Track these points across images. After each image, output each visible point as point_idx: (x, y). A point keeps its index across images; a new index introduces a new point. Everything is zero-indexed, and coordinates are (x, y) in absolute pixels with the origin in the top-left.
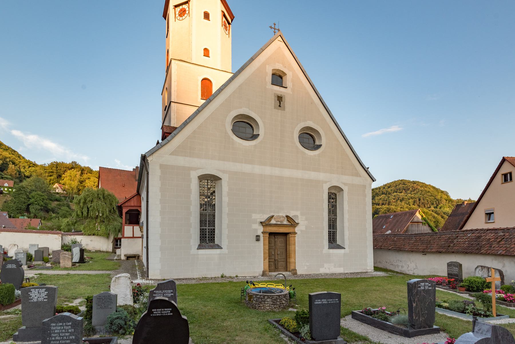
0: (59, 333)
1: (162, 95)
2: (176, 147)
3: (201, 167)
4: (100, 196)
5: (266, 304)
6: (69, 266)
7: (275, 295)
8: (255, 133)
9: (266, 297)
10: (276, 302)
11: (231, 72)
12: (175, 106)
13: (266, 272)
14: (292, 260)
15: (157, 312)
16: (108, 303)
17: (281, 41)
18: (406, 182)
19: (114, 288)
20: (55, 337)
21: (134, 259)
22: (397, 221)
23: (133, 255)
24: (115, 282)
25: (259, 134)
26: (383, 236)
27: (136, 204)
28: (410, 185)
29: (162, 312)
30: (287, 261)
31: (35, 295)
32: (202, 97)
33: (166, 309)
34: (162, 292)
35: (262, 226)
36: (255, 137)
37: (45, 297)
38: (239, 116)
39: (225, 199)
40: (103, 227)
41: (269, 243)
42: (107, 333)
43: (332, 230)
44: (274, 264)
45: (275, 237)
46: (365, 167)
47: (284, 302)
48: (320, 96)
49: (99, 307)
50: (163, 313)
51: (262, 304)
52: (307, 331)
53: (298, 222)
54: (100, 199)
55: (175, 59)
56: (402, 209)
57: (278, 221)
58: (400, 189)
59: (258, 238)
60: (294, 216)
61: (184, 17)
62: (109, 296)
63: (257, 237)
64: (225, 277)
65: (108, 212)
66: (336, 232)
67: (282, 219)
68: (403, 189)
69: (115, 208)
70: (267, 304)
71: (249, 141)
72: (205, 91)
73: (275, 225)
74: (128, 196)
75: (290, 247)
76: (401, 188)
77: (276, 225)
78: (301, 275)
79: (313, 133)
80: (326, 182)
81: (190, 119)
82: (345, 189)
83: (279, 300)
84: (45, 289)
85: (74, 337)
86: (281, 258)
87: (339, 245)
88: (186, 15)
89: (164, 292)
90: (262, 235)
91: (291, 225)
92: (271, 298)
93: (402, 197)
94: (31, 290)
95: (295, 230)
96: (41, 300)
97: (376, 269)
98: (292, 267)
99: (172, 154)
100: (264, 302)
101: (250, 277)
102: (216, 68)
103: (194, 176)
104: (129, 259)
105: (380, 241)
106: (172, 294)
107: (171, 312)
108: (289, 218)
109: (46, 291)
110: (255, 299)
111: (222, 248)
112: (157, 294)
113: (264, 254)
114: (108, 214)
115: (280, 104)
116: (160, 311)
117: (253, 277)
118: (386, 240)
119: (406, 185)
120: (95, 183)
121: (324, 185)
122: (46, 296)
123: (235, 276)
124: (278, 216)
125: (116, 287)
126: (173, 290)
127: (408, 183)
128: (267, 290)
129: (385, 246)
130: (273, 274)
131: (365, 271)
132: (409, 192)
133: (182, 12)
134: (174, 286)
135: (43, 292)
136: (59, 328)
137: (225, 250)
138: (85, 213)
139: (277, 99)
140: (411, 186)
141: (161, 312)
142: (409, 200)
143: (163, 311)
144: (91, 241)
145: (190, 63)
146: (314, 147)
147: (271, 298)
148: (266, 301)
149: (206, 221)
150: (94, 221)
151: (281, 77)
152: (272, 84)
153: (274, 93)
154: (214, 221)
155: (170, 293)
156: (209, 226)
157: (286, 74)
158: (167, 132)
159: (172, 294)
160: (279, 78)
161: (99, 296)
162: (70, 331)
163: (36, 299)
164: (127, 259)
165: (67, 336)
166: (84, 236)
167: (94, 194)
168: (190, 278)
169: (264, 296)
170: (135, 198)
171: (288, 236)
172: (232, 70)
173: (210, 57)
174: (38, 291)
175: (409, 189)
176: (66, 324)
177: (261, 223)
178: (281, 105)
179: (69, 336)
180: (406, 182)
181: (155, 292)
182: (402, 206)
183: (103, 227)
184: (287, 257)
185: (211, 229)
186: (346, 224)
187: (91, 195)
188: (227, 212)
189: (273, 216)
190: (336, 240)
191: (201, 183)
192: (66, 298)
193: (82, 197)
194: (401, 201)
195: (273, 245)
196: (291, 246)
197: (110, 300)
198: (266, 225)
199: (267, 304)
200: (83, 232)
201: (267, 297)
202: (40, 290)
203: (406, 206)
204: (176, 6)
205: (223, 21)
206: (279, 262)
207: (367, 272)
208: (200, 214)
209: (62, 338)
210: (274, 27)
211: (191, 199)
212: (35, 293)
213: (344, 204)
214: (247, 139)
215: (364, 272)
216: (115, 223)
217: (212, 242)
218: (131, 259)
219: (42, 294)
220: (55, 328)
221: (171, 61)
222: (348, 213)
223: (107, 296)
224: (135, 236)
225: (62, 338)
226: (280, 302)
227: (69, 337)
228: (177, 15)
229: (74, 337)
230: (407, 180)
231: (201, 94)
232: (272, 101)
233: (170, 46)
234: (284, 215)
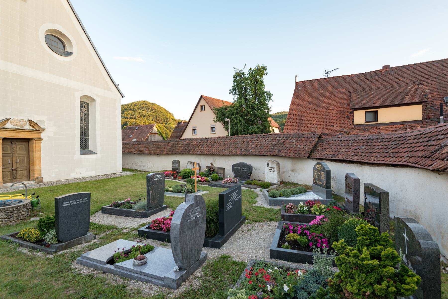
7: (10, 207)
14: (36, 168)
22: (141, 132)
30: (30, 169)
44: (11, 173)
45: (12, 143)
46: (116, 84)
57: (17, 126)
60: (39, 121)
66: (89, 139)
67: (22, 123)
68: (145, 108)
79: (62, 38)
83: (16, 212)
87: (91, 151)
92: (5, 212)
95: (40, 136)
97: (124, 169)
98: (36, 175)
108: (33, 122)
127: (149, 104)
132: (149, 111)
146: (64, 53)
147: (5, 212)
171: (31, 143)
175: (150, 108)
184: (30, 166)
194: (144, 117)
206: (18, 171)
234: (26, 119)
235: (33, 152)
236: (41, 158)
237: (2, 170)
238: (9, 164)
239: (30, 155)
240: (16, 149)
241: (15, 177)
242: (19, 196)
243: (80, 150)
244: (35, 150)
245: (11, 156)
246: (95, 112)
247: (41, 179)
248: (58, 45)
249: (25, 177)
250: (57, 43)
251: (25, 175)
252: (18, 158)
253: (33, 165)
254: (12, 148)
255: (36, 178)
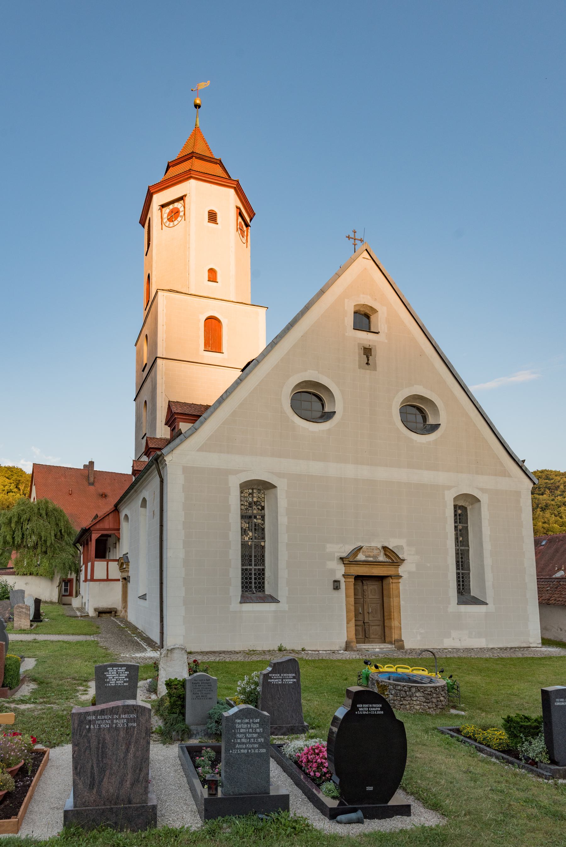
0: (245, 733)
1: (136, 345)
2: (206, 439)
3: (244, 469)
4: (41, 511)
5: (414, 702)
6: (27, 627)
7: (429, 687)
8: (327, 409)
9: (413, 690)
10: (432, 698)
11: (250, 303)
12: (163, 364)
13: (352, 644)
14: (395, 623)
15: (363, 709)
16: (206, 690)
17: (367, 259)
18: (550, 475)
19: (165, 667)
20: (241, 739)
21: (108, 615)
22: (557, 551)
23: (108, 608)
24: (167, 656)
25: (335, 412)
26: (550, 580)
27: (111, 526)
28: (559, 479)
29: (370, 710)
30: (385, 624)
31: (113, 675)
32: (206, 348)
33: (374, 705)
34: (280, 676)
35: (343, 565)
36: (327, 416)
37: (125, 680)
38: (302, 385)
39: (283, 520)
40: (46, 563)
41: (355, 595)
42: (207, 737)
43: (460, 571)
44: (362, 628)
45: (363, 583)
46: (519, 460)
47: (442, 698)
48: (435, 342)
49: (195, 696)
50: (371, 711)
51: (407, 701)
52: (541, 750)
53: (403, 557)
54: (41, 516)
55: (162, 290)
56: (546, 525)
57: (369, 556)
58: (539, 488)
59: (336, 585)
60: (396, 546)
61: (176, 222)
62: (207, 680)
63: (336, 583)
64: (285, 650)
65: (53, 538)
66: (469, 574)
67: (375, 552)
68: (546, 487)
69: (63, 531)
70: (415, 701)
71: (319, 424)
72: (210, 338)
73: (364, 563)
74: (101, 514)
75: (390, 602)
76: (541, 486)
77: (366, 563)
78: (412, 651)
79: (422, 405)
80: (449, 488)
81: (228, 394)
82: (484, 498)
83: (435, 695)
84: (125, 668)
85: (262, 740)
86: (375, 619)
87: (474, 597)
88: (179, 219)
89: (283, 677)
90: (342, 580)
91: (392, 563)
92: (422, 692)
93: (544, 502)
94: (108, 669)
95: (398, 571)
96: (121, 683)
97: (546, 642)
98: (395, 636)
99: (201, 449)
100: (410, 697)
101: (326, 651)
102: (228, 299)
103: (235, 483)
104: (101, 615)
105: (544, 589)
106: (295, 680)
107: (381, 710)
108: (389, 550)
109: (126, 670)
110: (393, 692)
111: (278, 602)
112: (273, 679)
113: (347, 612)
114: (53, 541)
115: (368, 360)
116: (368, 707)
117: (331, 651)
118: (557, 588)
119: (552, 479)
120: (4, 486)
121: (446, 492)
122: (126, 677)
123: (301, 650)
124: (369, 548)
125: (168, 664)
126: (296, 674)
127: (556, 476)
128: (399, 676)
129: (558, 599)
130: (364, 647)
131: (525, 645)
132: (558, 492)
133: (173, 214)
134: (297, 668)
135: (122, 672)
136: (245, 726)
137: (283, 605)
138: (18, 540)
139: (363, 352)
140: (561, 482)
141: (368, 709)
142: (559, 507)
143: (371, 707)
144: (26, 584)
145: (186, 294)
146: (425, 428)
147: (422, 692)
148: (415, 695)
149: (251, 556)
150: (31, 551)
151: (368, 316)
152: (354, 329)
153: (358, 344)
154: (263, 556)
155: (292, 679)
156: (255, 565)
157: (377, 311)
158: (178, 413)
159: (295, 680)
160: (365, 319)
161: (195, 680)
162: (258, 730)
163: (113, 682)
164: (99, 616)
165: (254, 738)
166: (17, 576)
167: (32, 507)
168: (229, 650)
169: (410, 688)
170: (111, 516)
171: (385, 582)
172: (252, 298)
173: (218, 282)
174: (117, 670)
175: (559, 487)
176: (253, 720)
177: (342, 559)
178: (370, 362)
179: (257, 738)
180: (550, 475)
181: (270, 675)
182: (546, 520)
183: (45, 561)
184: (385, 619)
185: (259, 570)
186: (488, 561)
187: (29, 509)
188: (287, 542)
189: (362, 548)
190: (470, 589)
191: (243, 495)
192: (74, 679)
193: (15, 513)
194: (543, 510)
195: (360, 597)
196: (392, 599)
197: (209, 685)
198: (349, 563)
199: (415, 701)
200: (14, 570)
201: (414, 689)
202: (119, 669)
203: (553, 519)
204: (163, 206)
205: (239, 222)
206: (370, 627)
207: (530, 647)
208: (242, 544)
209: (248, 740)
210: (353, 237)
211: (230, 522)
212: (113, 673)
213: (483, 525)
214: (314, 420)
215: (524, 648)
216: (64, 555)
217: (260, 591)
218: (104, 615)
219: (121, 675)
220: (240, 726)
221: (157, 292)
222: (490, 541)
223: (205, 680)
224: (110, 578)
225: (248, 740)
226: (436, 698)
227: (257, 740)
228: (165, 220)
229: (262, 740)
230: (553, 470)
231: (205, 343)
232: (356, 356)
233: (154, 269)
234: (379, 546)
235: (389, 597)
236: (400, 607)
237: (355, 623)
238: (360, 615)
239: (384, 603)
240: (368, 591)
241: (367, 636)
242: (420, 670)
243: (458, 595)
244: (392, 594)
245: (363, 602)
246: (481, 522)
247: (401, 642)
248: (416, 419)
249: (380, 637)
250: (414, 415)
251: (379, 633)
252: (370, 607)
253: (390, 619)
254: (363, 590)
255: (395, 641)
